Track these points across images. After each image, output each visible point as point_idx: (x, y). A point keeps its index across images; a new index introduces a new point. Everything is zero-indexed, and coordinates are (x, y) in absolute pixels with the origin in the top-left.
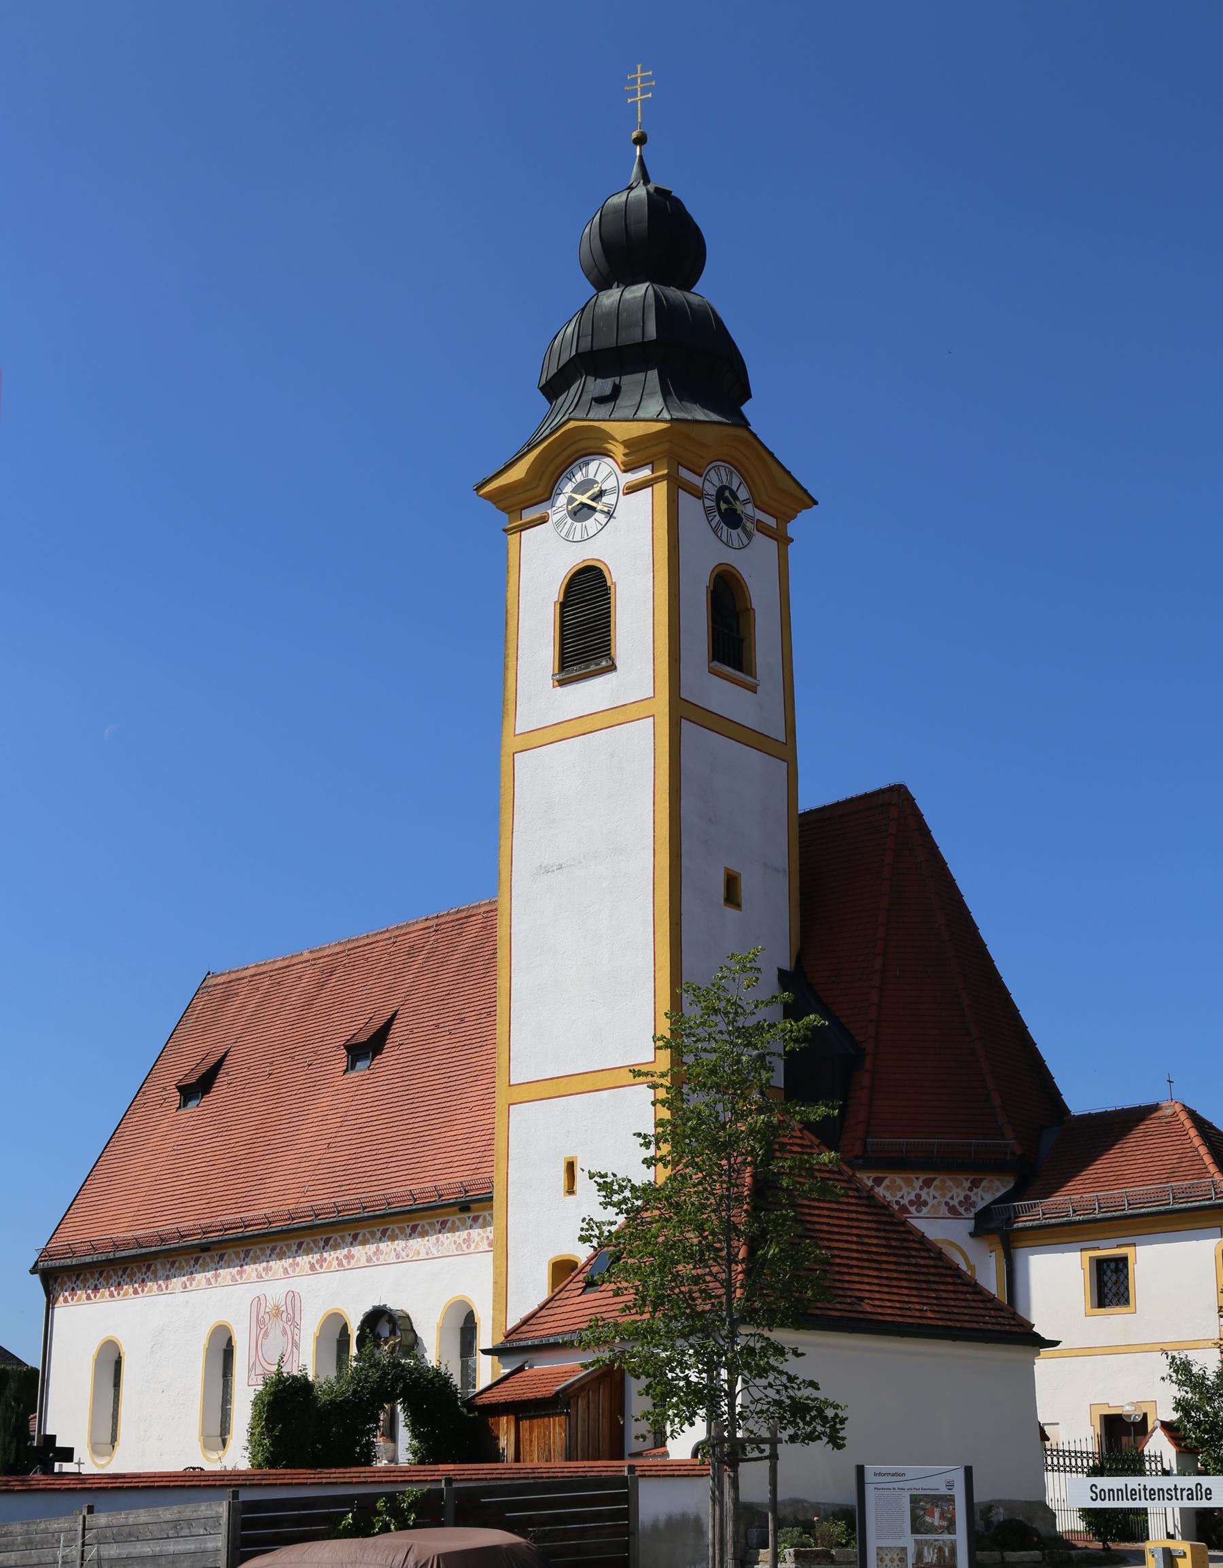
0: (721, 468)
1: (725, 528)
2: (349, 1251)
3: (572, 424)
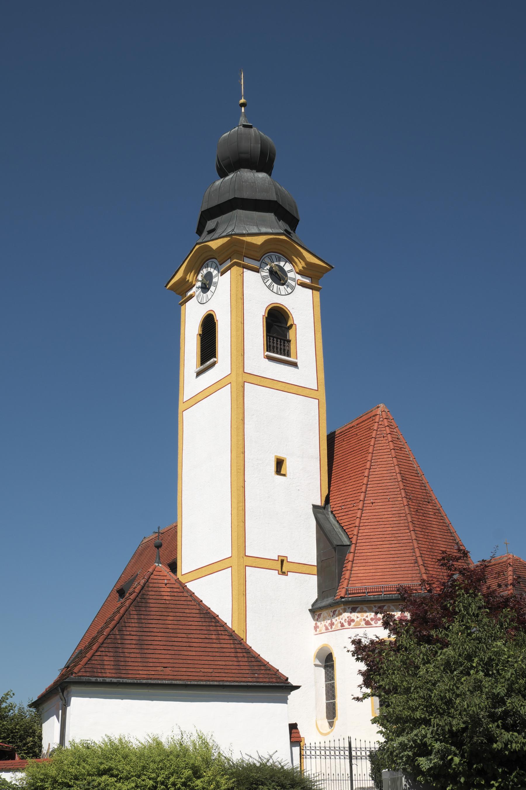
0: (272, 256)
1: (275, 285)
2: (332, 621)
3: (197, 247)
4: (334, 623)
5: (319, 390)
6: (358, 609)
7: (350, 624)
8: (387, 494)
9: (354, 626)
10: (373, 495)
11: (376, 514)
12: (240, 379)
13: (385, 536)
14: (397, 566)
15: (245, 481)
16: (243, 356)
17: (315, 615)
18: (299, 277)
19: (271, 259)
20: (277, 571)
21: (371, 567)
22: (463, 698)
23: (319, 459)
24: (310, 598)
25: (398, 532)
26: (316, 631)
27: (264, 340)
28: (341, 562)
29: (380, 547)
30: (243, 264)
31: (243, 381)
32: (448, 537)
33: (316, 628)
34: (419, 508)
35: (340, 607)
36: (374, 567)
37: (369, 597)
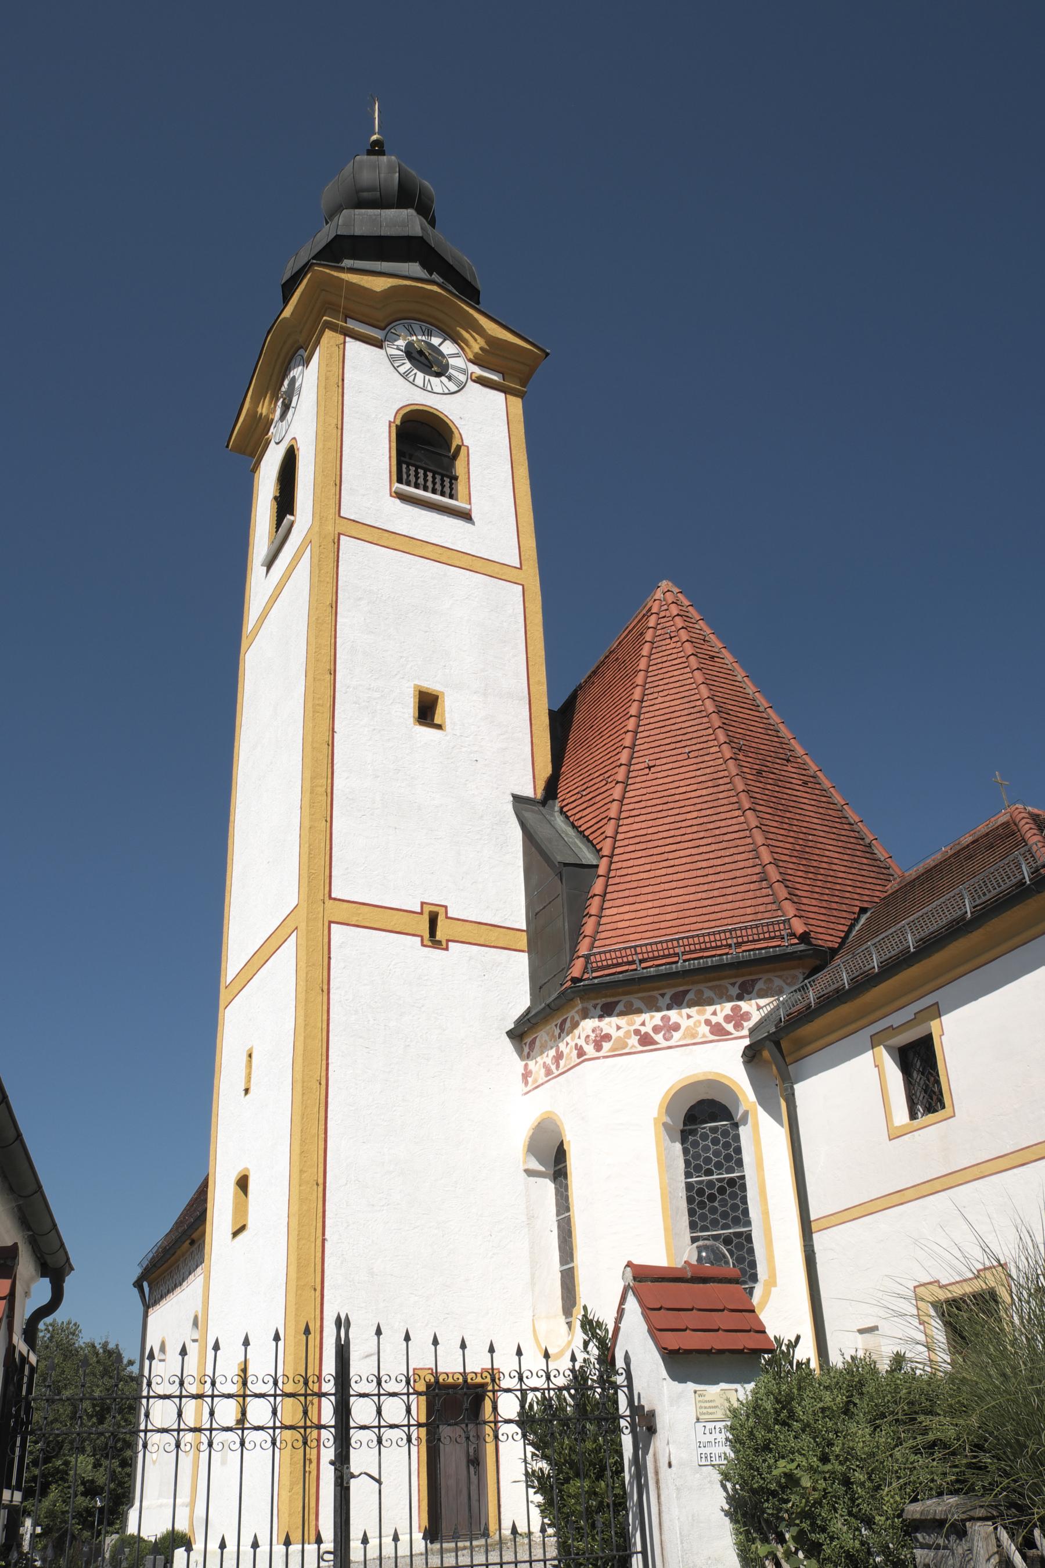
4: (562, 1052)
5: (523, 567)
6: (620, 1007)
7: (598, 1047)
8: (683, 744)
9: (610, 1051)
10: (652, 751)
11: (659, 788)
12: (330, 528)
13: (683, 831)
14: (716, 893)
15: (333, 731)
16: (338, 487)
17: (524, 1046)
18: (477, 371)
19: (411, 329)
20: (419, 939)
21: (649, 904)
22: (899, 1516)
23: (527, 702)
24: (510, 1006)
25: (715, 818)
26: (526, 1083)
27: (390, 465)
28: (577, 911)
29: (671, 856)
30: (342, 327)
31: (336, 532)
32: (844, 832)
33: (526, 1075)
34: (765, 769)
35: (573, 1008)
36: (656, 903)
37: (645, 971)
